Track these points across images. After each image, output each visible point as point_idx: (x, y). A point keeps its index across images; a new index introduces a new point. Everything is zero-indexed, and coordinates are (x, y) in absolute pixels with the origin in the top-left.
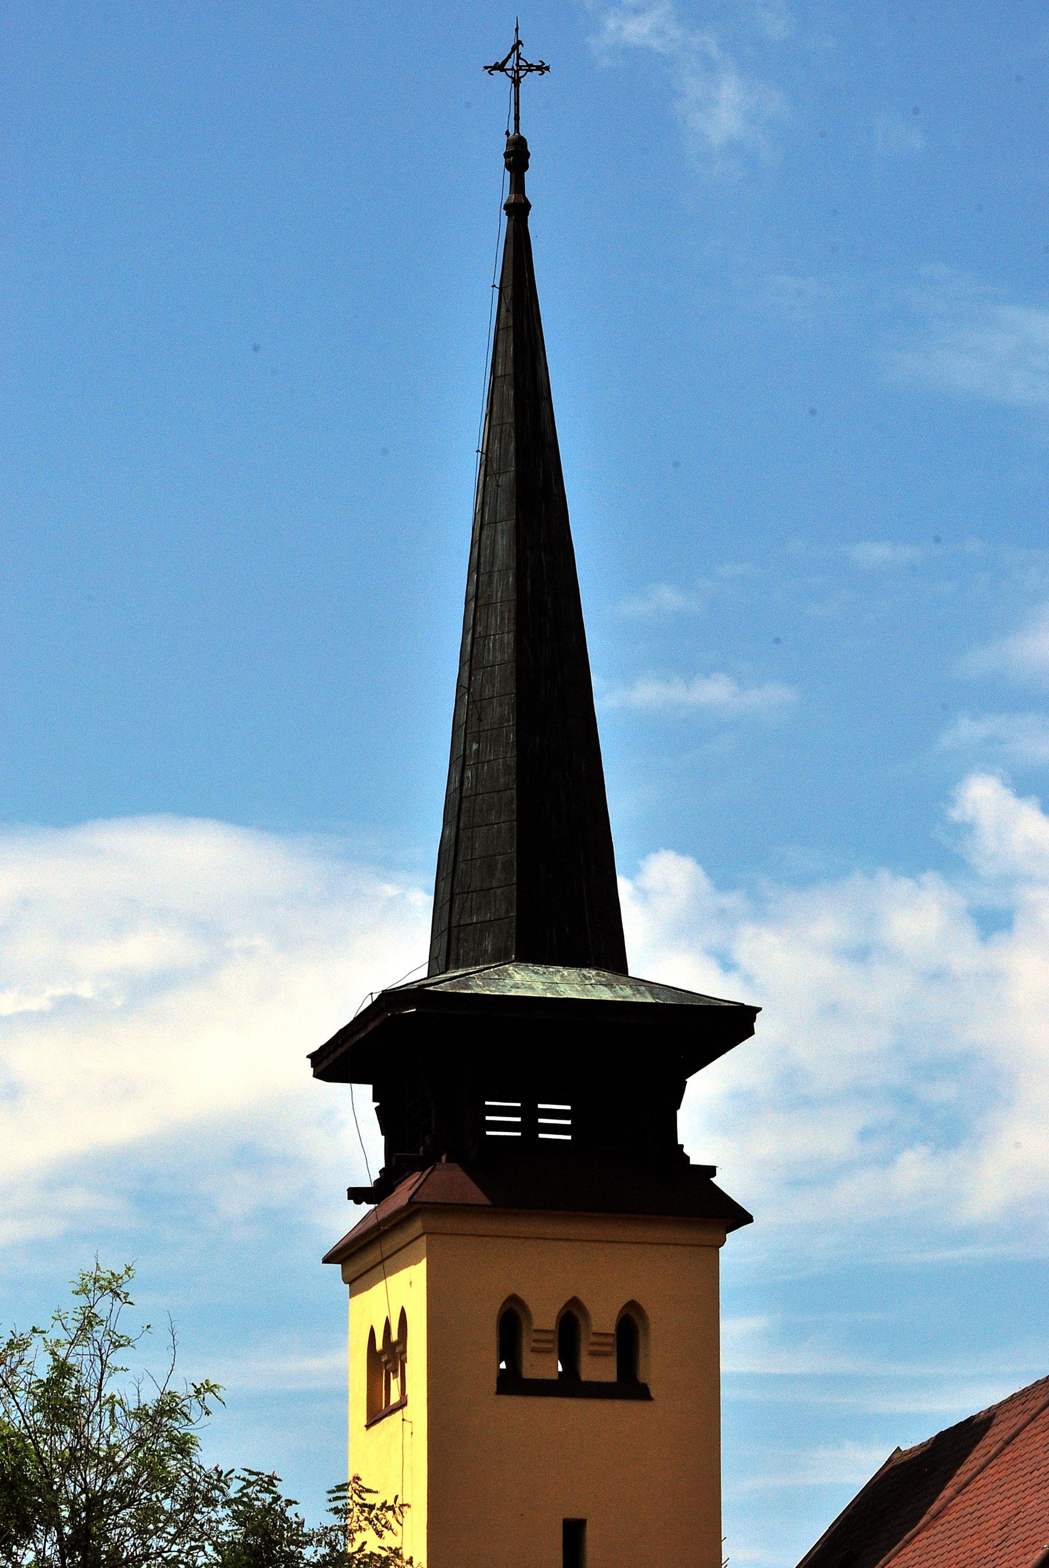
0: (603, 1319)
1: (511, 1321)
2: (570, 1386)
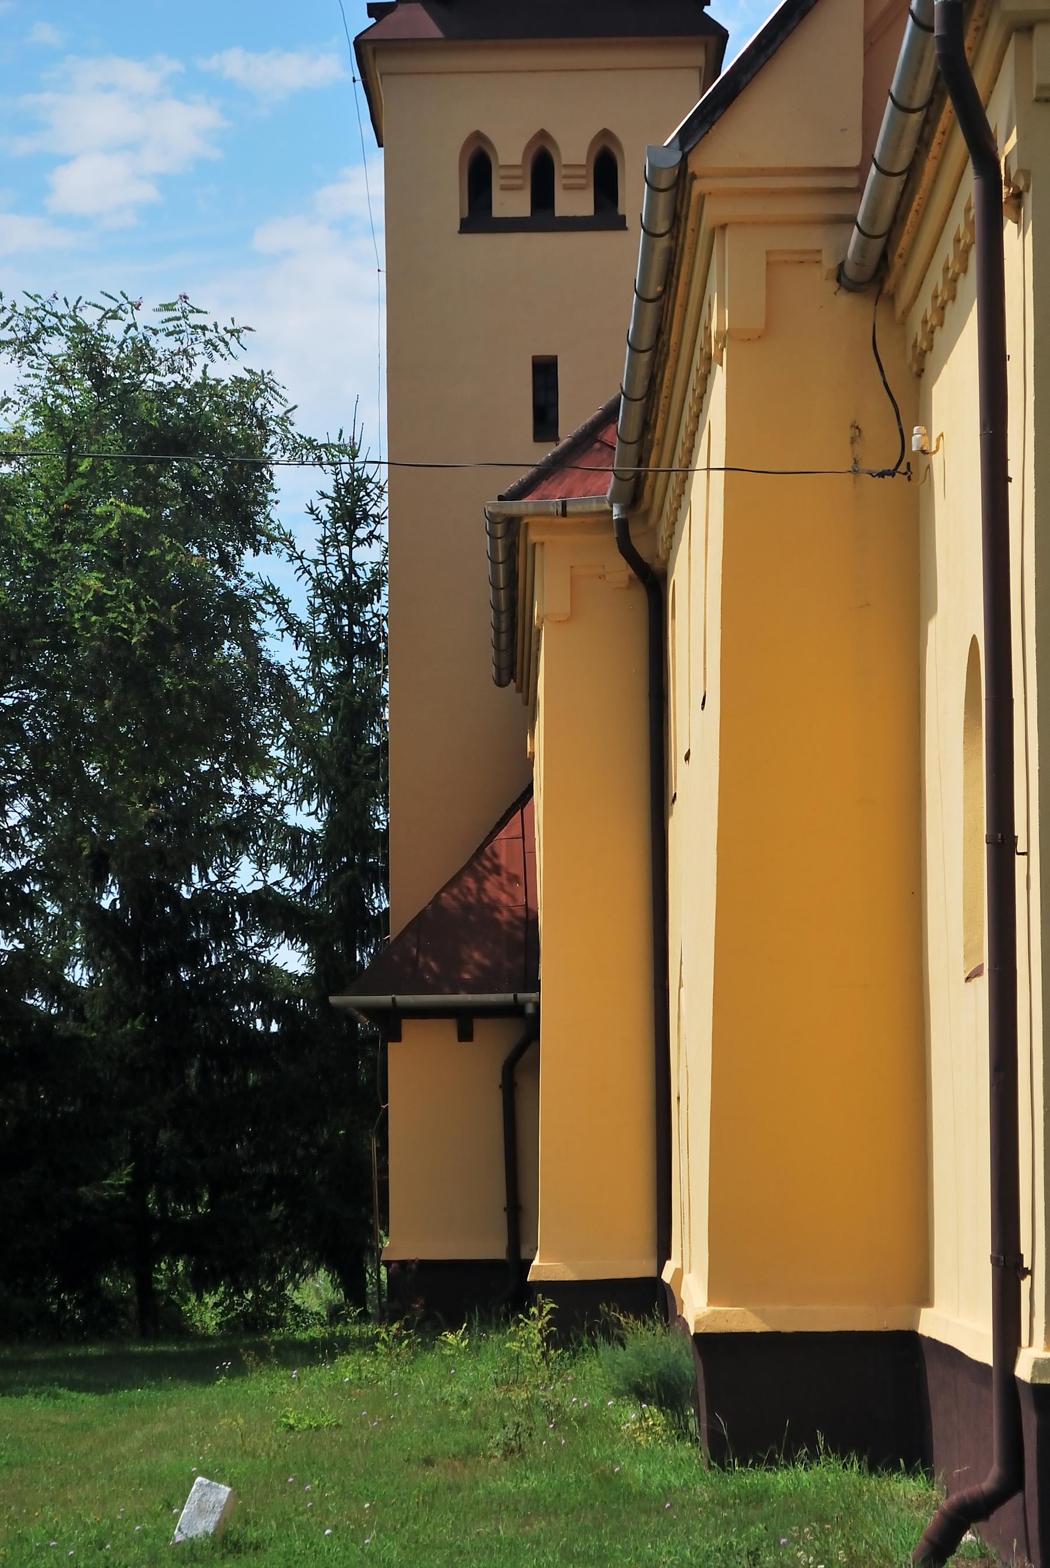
0: (573, 152)
1: (479, 170)
2: (543, 215)
